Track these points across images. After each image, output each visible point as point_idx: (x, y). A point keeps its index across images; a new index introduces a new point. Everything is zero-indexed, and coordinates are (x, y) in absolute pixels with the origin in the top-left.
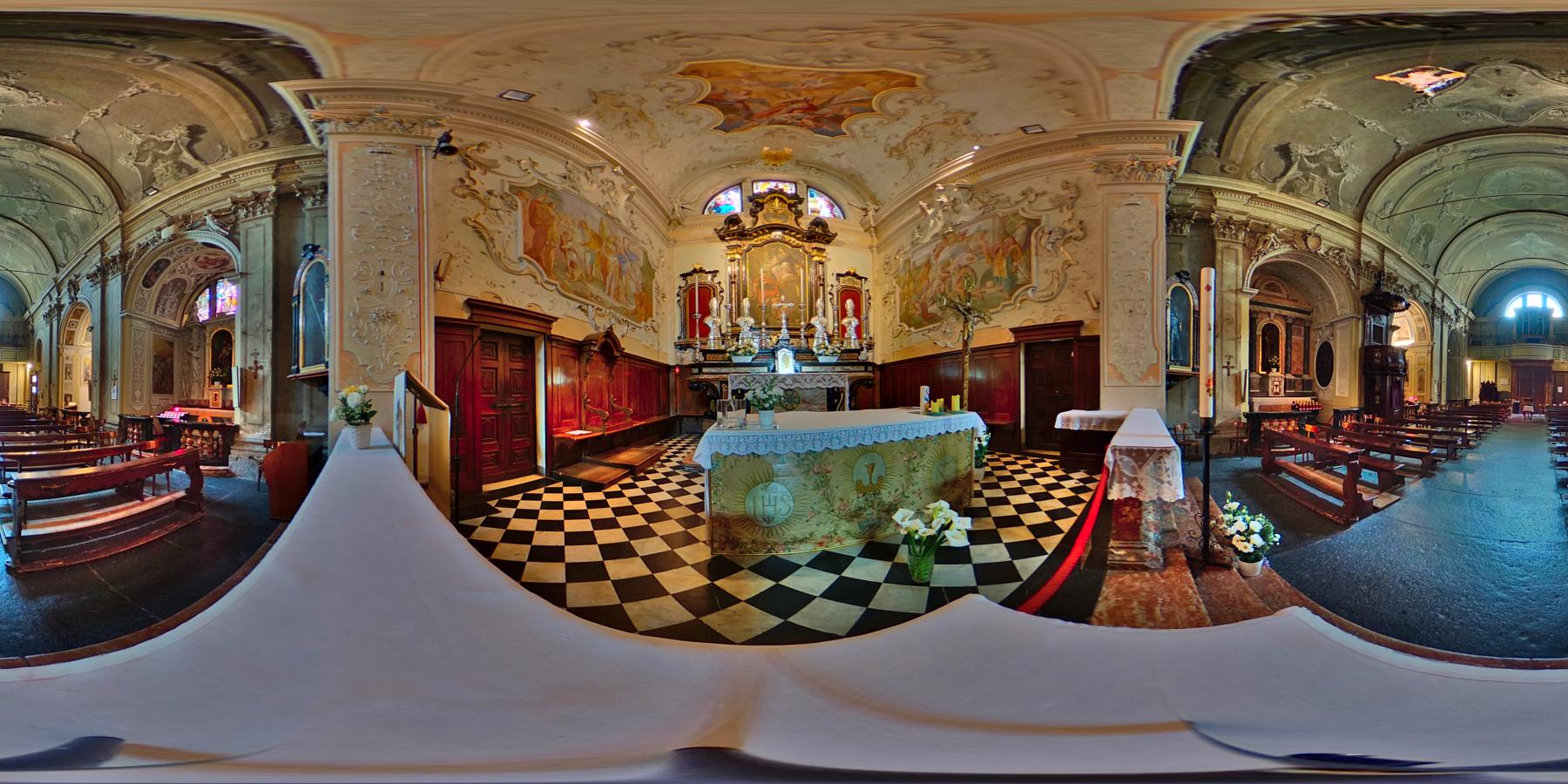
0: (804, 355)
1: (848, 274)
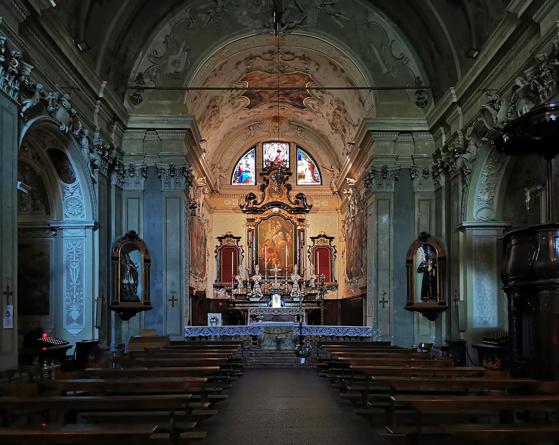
0: (285, 296)
1: (320, 236)
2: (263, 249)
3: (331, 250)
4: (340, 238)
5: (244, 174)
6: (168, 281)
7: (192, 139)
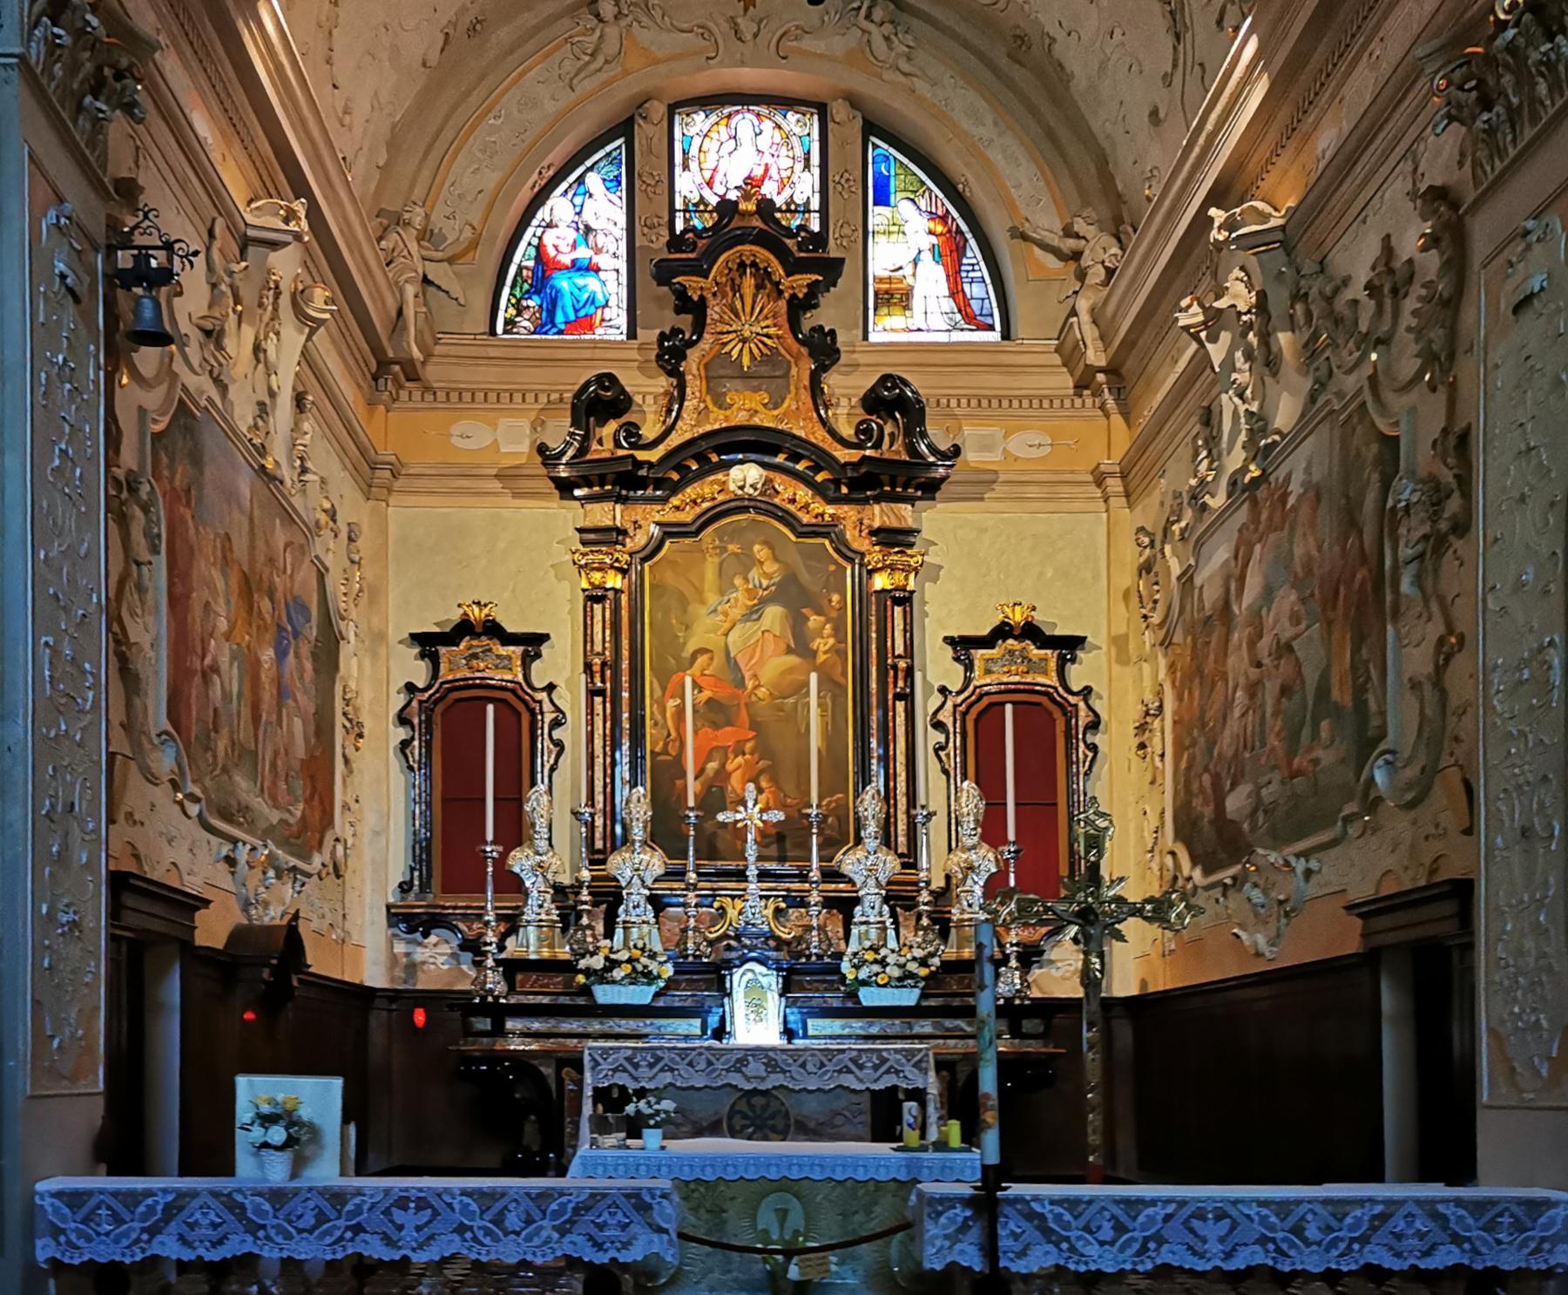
0: (807, 977)
1: (1002, 631)
2: (671, 704)
3: (1070, 713)
4: (1119, 642)
5: (562, 282)
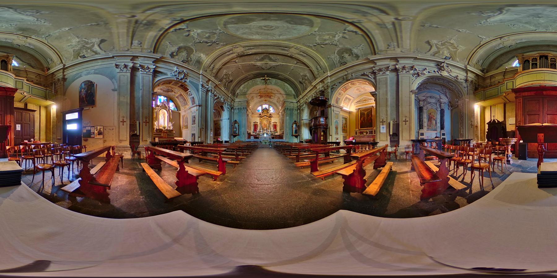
0: (267, 134)
6: (243, 130)
7: (248, 102)
